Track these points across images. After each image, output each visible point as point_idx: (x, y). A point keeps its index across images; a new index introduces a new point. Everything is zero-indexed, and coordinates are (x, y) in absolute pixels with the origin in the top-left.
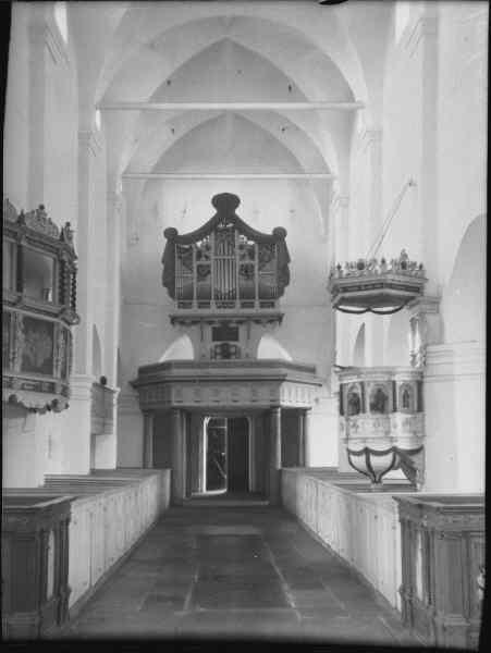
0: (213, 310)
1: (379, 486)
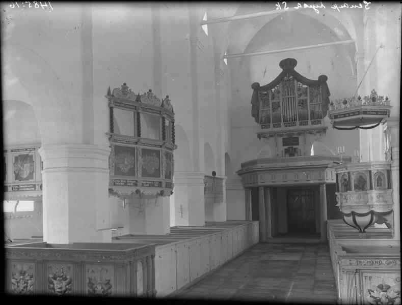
0: (283, 128)
1: (364, 234)
